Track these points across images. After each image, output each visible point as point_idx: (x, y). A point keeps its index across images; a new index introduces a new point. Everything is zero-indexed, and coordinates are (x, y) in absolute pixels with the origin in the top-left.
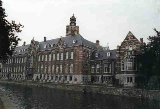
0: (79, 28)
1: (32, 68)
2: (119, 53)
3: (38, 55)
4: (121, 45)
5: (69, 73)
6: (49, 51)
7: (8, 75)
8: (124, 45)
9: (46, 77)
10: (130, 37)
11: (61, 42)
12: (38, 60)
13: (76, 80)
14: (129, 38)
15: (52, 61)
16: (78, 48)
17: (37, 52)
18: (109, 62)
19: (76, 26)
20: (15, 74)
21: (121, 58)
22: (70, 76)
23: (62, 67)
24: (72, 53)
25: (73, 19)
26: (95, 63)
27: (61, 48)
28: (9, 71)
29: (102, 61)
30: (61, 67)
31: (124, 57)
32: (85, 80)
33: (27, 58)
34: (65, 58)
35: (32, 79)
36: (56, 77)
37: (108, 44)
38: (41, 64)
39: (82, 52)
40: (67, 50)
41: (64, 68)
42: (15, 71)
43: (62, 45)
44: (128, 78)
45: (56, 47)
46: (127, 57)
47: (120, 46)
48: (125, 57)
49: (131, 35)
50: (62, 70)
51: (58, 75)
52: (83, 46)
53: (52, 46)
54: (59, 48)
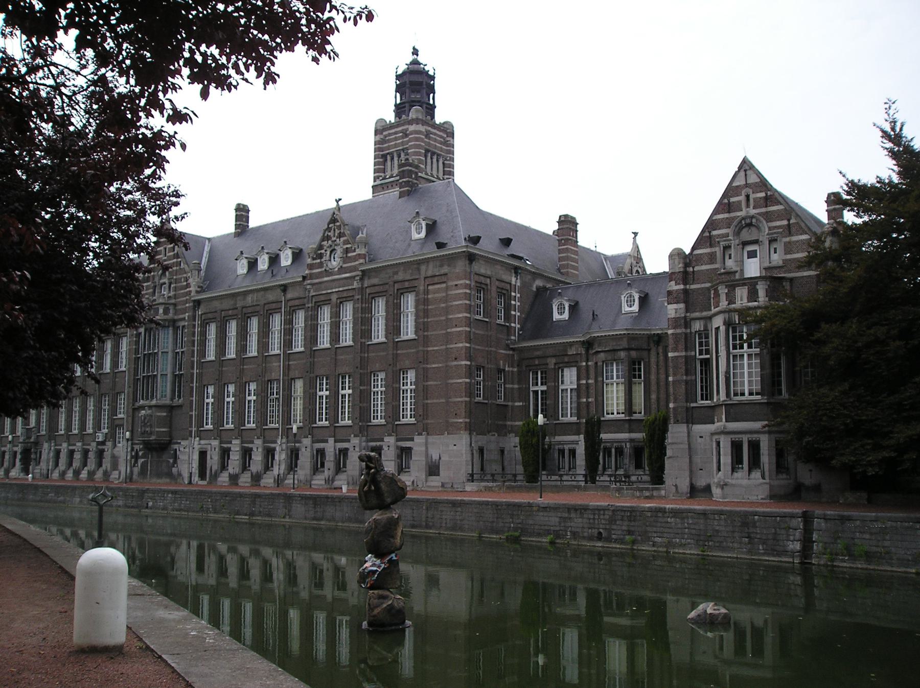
0: (452, 135)
1: (167, 401)
2: (686, 297)
3: (205, 324)
4: (693, 248)
5: (393, 425)
6: (271, 297)
7: (26, 453)
8: (711, 246)
9: (258, 457)
10: (748, 197)
11: (340, 236)
12: (202, 353)
13: (433, 469)
14: (740, 202)
15: (288, 357)
16: (445, 269)
17: (198, 303)
18: (634, 354)
19: (434, 126)
20: (65, 445)
21: (697, 326)
22: (397, 447)
23: (348, 392)
24: (409, 303)
25: (415, 78)
26: (552, 362)
27: (342, 270)
28: (29, 430)
29: (588, 344)
30: (342, 392)
31: (710, 318)
32: (187, 458)
33: (137, 343)
34: (397, 331)
35: (170, 475)
36: (318, 451)
37: (636, 234)
38: (220, 373)
39: (468, 297)
40: (375, 281)
41: (363, 399)
42: (69, 427)
43: (347, 251)
44: (736, 447)
45: (311, 267)
46: (727, 315)
47: (688, 251)
48: (718, 322)
49: (753, 179)
50: (353, 407)
51: (327, 441)
52: (471, 258)
53: (286, 260)
54: (328, 273)
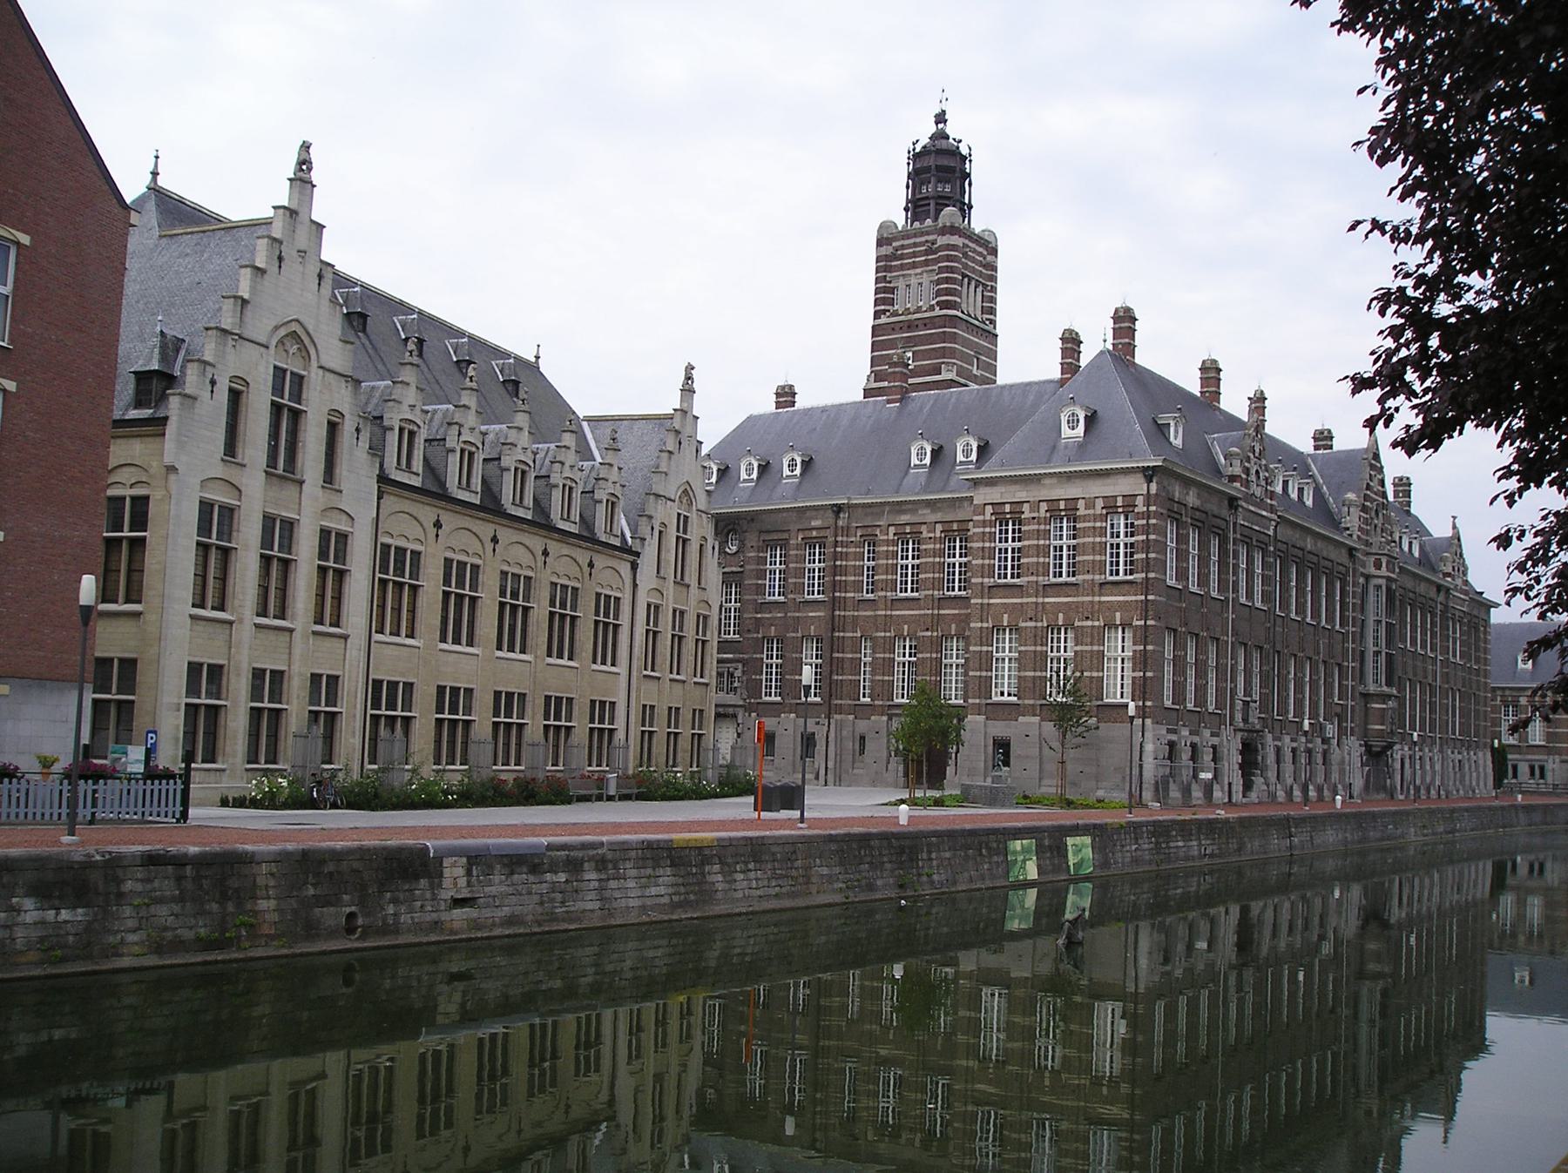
0: (994, 252)
